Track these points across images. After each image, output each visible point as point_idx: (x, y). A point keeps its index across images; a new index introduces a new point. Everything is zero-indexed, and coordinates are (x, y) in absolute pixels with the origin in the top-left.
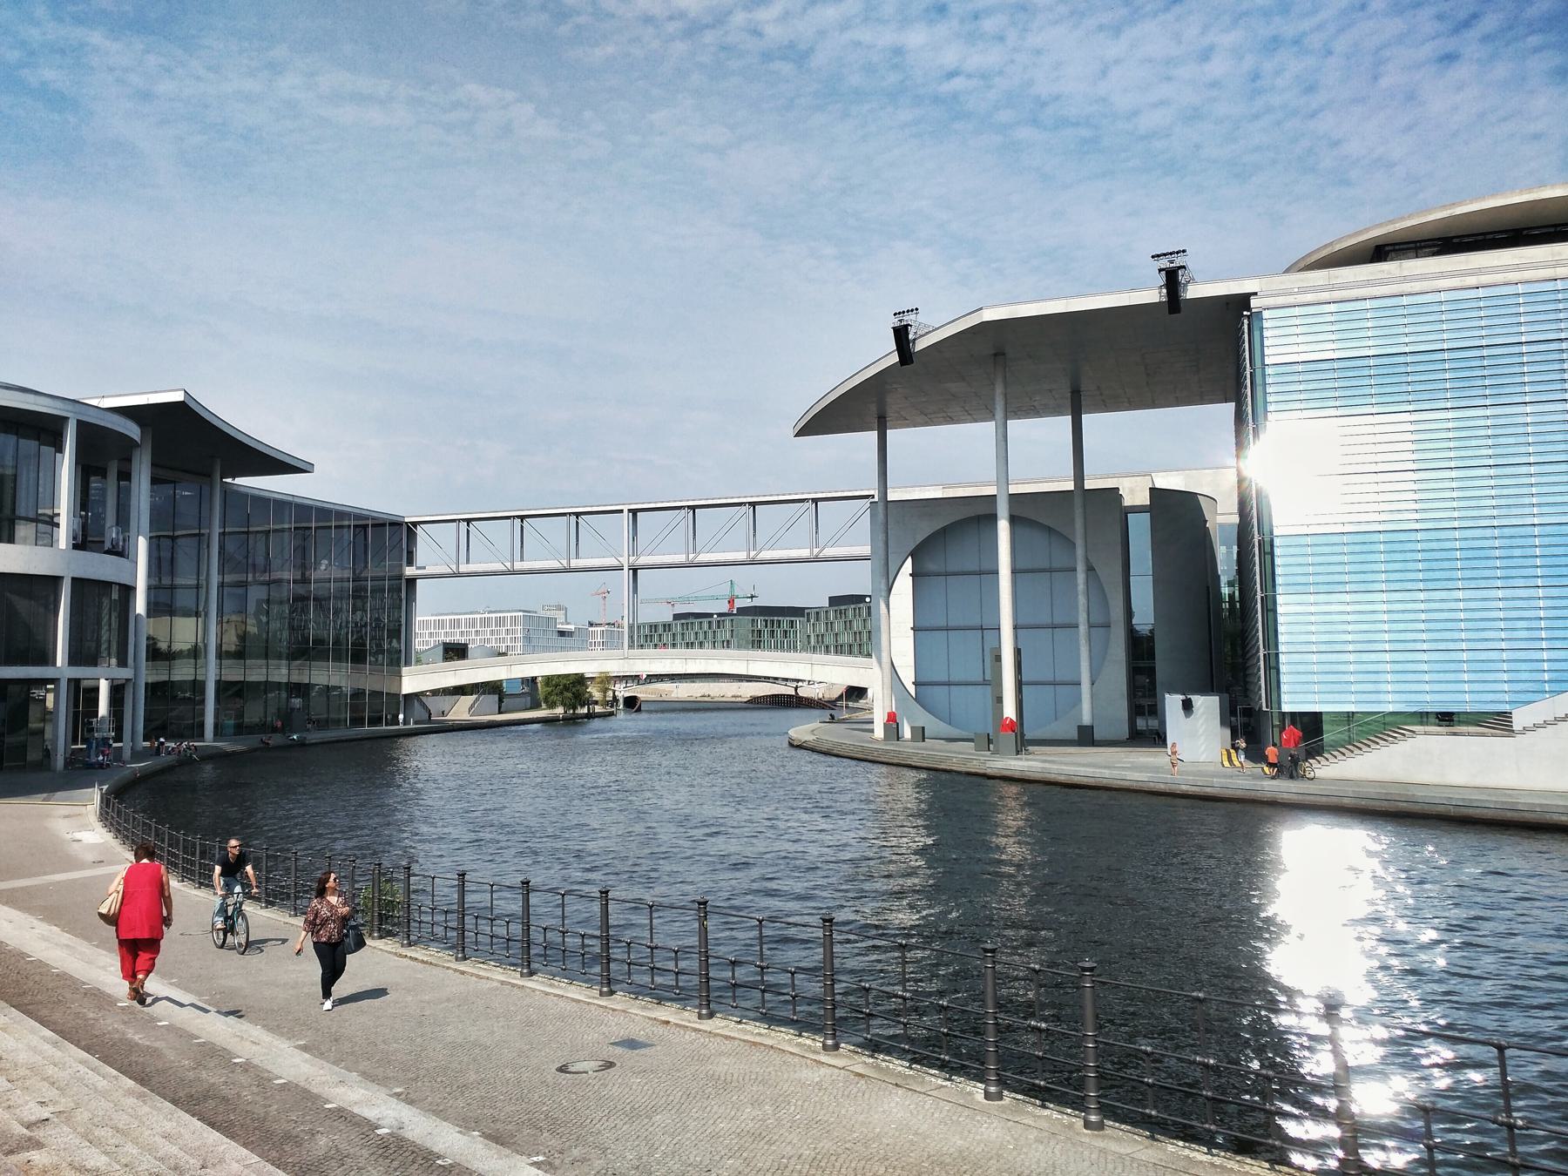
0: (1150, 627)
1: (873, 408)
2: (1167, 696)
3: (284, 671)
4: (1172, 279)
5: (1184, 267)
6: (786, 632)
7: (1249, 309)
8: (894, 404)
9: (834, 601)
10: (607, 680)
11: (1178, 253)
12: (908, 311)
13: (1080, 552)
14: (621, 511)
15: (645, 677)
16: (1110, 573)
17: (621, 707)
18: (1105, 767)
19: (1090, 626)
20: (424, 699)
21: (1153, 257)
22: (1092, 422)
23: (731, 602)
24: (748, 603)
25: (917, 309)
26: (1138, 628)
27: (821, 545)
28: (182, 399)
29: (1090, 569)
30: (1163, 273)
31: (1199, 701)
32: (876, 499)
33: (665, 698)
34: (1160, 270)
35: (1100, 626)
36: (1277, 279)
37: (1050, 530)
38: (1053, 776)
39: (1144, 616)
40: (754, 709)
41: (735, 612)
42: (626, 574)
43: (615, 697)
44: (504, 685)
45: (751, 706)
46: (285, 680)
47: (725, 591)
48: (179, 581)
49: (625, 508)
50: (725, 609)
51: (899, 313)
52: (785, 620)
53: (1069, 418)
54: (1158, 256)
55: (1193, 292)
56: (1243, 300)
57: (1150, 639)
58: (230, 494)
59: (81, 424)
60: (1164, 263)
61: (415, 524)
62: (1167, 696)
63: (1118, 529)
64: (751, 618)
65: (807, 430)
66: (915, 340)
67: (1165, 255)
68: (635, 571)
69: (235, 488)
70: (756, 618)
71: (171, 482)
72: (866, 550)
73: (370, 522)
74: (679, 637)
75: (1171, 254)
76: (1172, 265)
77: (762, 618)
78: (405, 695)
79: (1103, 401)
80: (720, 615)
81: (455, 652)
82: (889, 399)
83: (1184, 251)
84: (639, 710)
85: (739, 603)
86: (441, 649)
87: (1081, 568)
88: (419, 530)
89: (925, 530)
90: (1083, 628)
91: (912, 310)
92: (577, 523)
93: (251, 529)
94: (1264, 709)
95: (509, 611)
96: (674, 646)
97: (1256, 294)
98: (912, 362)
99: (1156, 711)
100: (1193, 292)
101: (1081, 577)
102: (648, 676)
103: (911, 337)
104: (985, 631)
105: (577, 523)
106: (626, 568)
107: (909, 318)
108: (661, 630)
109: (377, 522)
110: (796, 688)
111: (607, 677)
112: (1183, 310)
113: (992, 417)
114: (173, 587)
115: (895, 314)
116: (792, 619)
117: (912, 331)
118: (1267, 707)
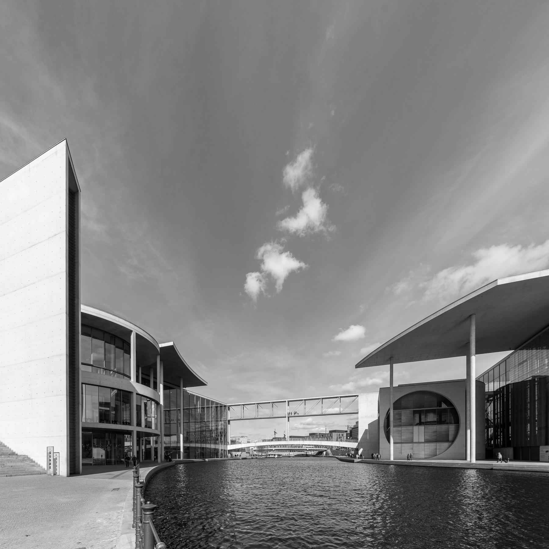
22: (176, 446)
42: (287, 418)
49: (287, 400)
58: (185, 392)
59: (137, 334)
65: (358, 366)
73: (219, 405)
92: (258, 406)
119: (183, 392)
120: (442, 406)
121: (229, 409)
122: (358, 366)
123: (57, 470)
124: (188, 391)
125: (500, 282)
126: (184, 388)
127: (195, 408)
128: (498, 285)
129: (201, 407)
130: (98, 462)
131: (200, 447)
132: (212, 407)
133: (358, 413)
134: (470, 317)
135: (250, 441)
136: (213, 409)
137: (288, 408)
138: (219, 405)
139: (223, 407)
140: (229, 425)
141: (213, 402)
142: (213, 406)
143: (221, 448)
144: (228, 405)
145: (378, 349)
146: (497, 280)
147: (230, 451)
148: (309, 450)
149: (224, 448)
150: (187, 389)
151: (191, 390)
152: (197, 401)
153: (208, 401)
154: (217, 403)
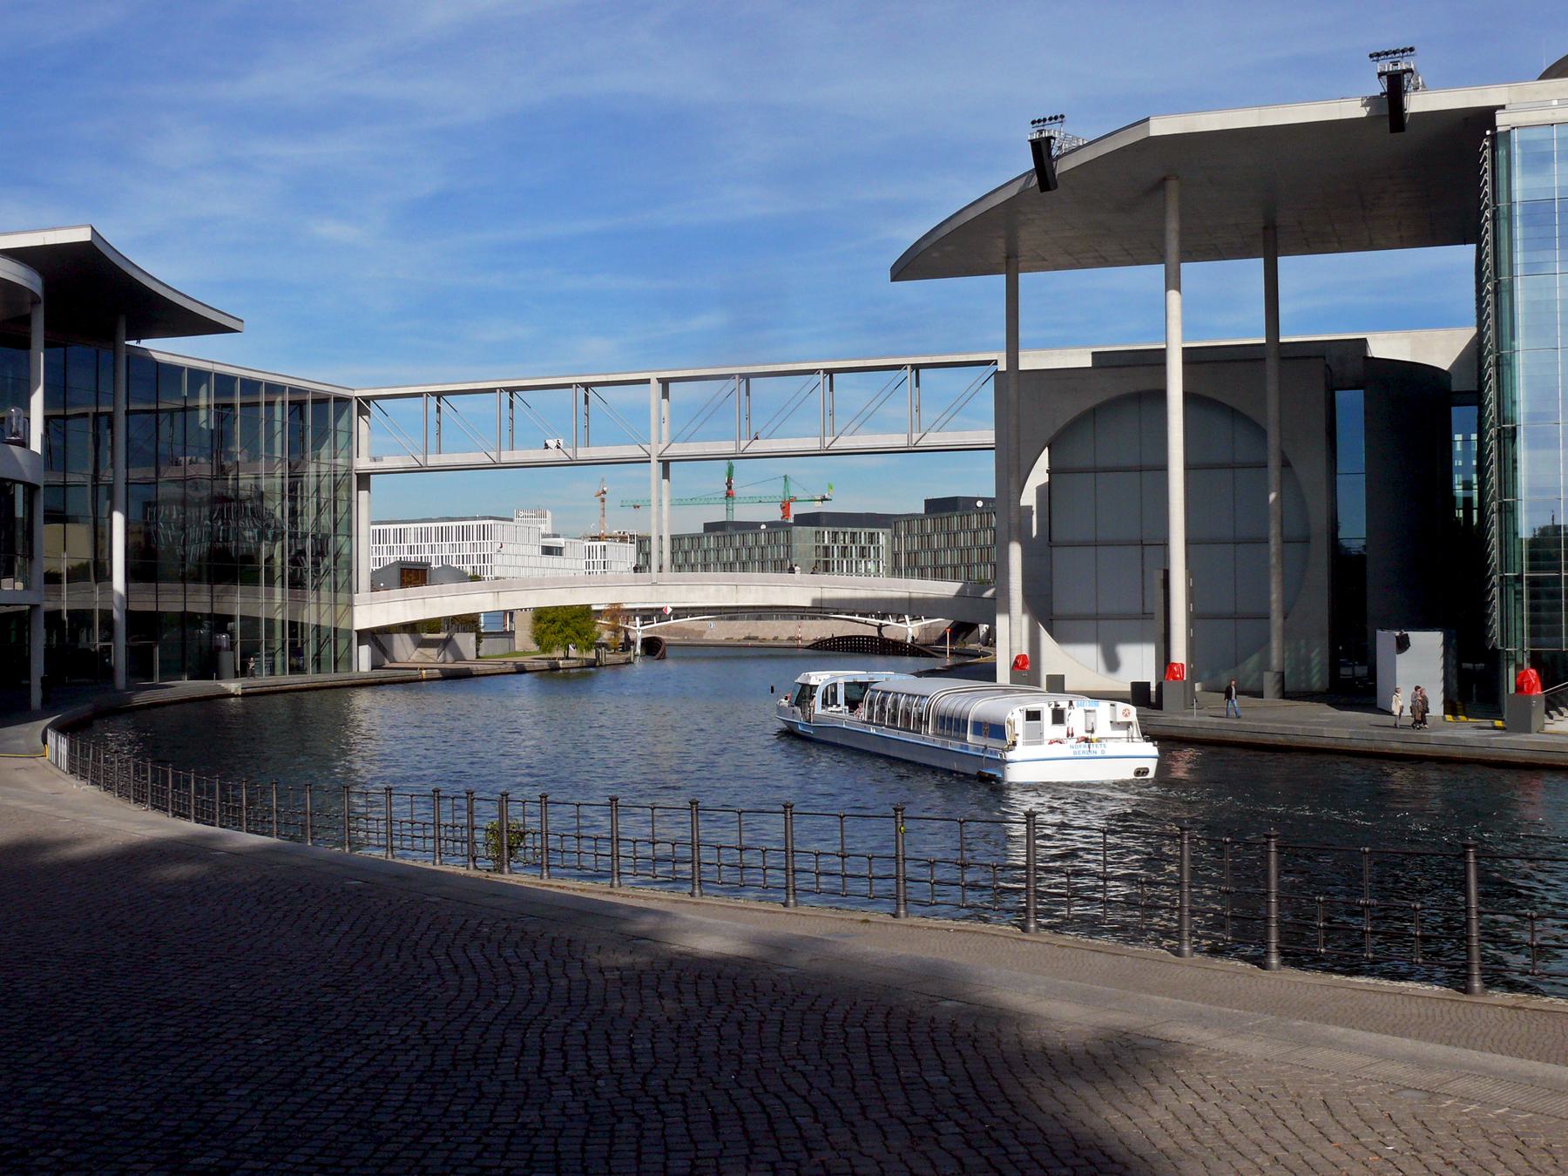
0: (1363, 542)
1: (1001, 244)
2: (1379, 632)
3: (206, 598)
4: (1396, 85)
5: (1410, 71)
6: (863, 548)
7: (1494, 128)
8: (1028, 238)
9: (933, 506)
10: (617, 613)
11: (1403, 51)
12: (1050, 119)
13: (1273, 441)
14: (647, 381)
15: (669, 610)
16: (1311, 470)
17: (638, 651)
18: (1297, 723)
19: (1285, 541)
20: (379, 637)
21: (1371, 56)
22: (1287, 265)
23: (785, 508)
24: (817, 507)
25: (1062, 116)
26: (1345, 543)
27: (924, 428)
28: (89, 239)
29: (1285, 464)
30: (1385, 77)
31: (1415, 637)
32: (1002, 367)
33: (694, 640)
34: (1380, 75)
35: (1295, 541)
36: (904, 677)
37: (1233, 413)
38: (1232, 734)
39: (1354, 530)
40: (814, 656)
41: (791, 520)
43: (627, 638)
44: (482, 619)
45: (816, 652)
46: (207, 610)
47: (778, 491)
48: (72, 478)
49: (653, 376)
50: (775, 514)
51: (1039, 121)
52: (863, 532)
53: (1262, 260)
54: (1378, 55)
55: (1416, 103)
56: (1487, 116)
57: (1360, 560)
58: (144, 358)
60: (1386, 66)
61: (368, 400)
62: (1379, 632)
63: (1322, 410)
64: (814, 529)
65: (910, 267)
66: (1058, 157)
67: (1387, 54)
68: (666, 464)
69: (140, 353)
70: (821, 529)
71: (60, 346)
72: (988, 436)
74: (712, 555)
75: (1395, 52)
76: (1395, 68)
77: (831, 529)
78: (357, 631)
79: (1306, 239)
80: (769, 524)
81: (413, 575)
82: (1023, 234)
83: (1411, 49)
84: (663, 657)
85: (796, 509)
86: (396, 574)
87: (1274, 463)
88: (373, 408)
89: (1071, 408)
90: (1274, 545)
91: (1056, 118)
92: (586, 397)
93: (162, 406)
94: (1500, 648)
95: (475, 519)
96: (706, 568)
97: (1503, 107)
98: (1056, 187)
99: (1366, 655)
100: (1416, 103)
101: (1274, 472)
102: (674, 609)
103: (1054, 152)
104: (1146, 548)
105: (586, 397)
106: (654, 459)
107: (1052, 130)
108: (686, 545)
109: (317, 397)
110: (880, 627)
111: (619, 610)
112: (1407, 130)
113: (1160, 258)
114: (65, 486)
115: (1033, 122)
116: (872, 530)
117: (1055, 144)
118: (1502, 645)
119: (128, 358)
120: (1029, 504)
121: (362, 411)
122: (910, 267)
123: (78, 767)
124: (157, 356)
125: (1161, 126)
126: (133, 343)
127: (185, 409)
128: (1153, 133)
129: (212, 402)
130: (1063, 846)
131: (210, 616)
132: (270, 404)
133: (649, 462)
134: (1161, 184)
135: (560, 542)
136: (278, 416)
137: (665, 413)
138: (309, 397)
139: (332, 405)
140: (363, 494)
141: (273, 388)
142: (279, 399)
143: (313, 621)
144: (357, 393)
145: (982, 203)
146: (1148, 119)
147: (377, 638)
148: (679, 612)
149: (336, 622)
150: (145, 343)
151: (164, 349)
152: (194, 392)
153: (250, 386)
154: (293, 390)
